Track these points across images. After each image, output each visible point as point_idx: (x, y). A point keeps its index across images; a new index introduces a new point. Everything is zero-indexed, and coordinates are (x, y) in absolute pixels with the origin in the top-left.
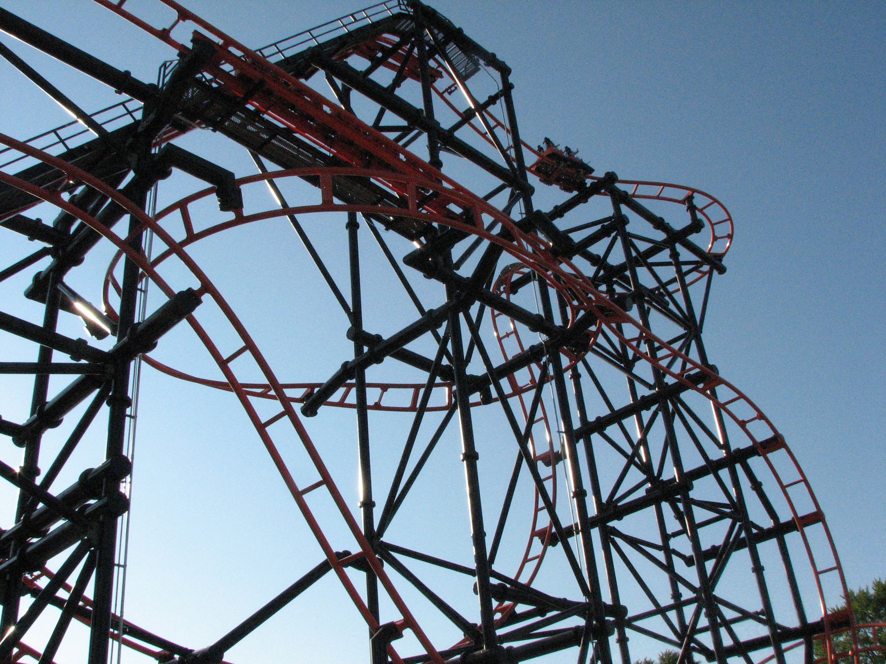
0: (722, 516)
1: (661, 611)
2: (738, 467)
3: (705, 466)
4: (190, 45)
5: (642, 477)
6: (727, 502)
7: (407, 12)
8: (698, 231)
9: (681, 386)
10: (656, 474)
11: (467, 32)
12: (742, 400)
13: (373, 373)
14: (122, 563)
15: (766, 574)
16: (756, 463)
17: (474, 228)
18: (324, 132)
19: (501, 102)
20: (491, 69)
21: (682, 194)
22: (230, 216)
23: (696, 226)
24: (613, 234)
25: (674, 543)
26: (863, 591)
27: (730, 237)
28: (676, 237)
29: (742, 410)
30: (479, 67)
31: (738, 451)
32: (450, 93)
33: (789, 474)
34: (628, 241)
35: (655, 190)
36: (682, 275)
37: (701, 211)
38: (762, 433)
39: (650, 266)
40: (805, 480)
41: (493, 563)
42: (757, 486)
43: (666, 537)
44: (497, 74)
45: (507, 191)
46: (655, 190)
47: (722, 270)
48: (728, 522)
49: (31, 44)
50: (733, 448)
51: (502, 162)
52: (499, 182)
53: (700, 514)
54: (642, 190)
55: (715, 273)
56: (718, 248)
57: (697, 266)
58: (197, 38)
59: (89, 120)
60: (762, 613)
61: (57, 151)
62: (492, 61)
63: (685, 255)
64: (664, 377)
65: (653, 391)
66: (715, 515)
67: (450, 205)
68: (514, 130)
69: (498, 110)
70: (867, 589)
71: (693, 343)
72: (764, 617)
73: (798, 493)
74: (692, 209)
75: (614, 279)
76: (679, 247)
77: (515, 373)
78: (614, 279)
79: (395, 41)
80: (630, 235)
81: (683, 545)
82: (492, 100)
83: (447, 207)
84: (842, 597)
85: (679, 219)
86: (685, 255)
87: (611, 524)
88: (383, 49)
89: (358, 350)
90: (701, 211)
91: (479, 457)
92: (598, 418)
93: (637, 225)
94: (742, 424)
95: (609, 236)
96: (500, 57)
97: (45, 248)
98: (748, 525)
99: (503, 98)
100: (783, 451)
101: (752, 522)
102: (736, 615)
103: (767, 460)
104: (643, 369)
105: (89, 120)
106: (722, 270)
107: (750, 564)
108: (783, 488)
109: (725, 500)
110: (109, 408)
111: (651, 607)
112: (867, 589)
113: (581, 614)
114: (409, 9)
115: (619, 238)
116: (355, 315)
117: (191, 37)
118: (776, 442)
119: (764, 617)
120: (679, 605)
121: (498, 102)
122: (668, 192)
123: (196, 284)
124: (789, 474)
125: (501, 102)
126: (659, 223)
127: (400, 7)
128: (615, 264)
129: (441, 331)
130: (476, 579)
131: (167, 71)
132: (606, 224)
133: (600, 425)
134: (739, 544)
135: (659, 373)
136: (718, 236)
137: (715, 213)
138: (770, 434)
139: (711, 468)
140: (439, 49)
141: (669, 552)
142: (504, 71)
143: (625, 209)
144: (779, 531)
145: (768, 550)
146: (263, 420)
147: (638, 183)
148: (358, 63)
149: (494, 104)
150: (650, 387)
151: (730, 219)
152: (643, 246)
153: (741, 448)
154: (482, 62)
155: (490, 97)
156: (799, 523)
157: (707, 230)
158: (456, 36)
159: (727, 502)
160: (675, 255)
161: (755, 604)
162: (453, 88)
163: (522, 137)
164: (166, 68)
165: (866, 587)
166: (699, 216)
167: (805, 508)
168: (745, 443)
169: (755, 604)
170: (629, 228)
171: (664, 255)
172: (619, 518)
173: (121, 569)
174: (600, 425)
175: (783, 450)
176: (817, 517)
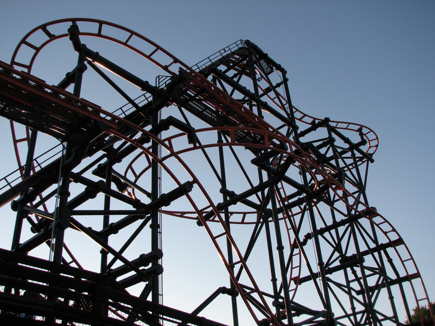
0: (375, 273)
1: (347, 316)
2: (382, 252)
3: (368, 250)
4: (178, 73)
5: (339, 255)
6: (377, 267)
7: (244, 46)
8: (364, 145)
9: (360, 216)
10: (344, 253)
11: (269, 56)
12: (386, 223)
13: (231, 208)
14: (161, 294)
15: (395, 300)
16: (390, 250)
17: (284, 151)
18: (216, 102)
19: (282, 87)
20: (278, 72)
21: (357, 127)
22: (192, 146)
23: (363, 142)
24: (328, 146)
25: (352, 285)
26: (423, 307)
27: (377, 146)
28: (353, 147)
29: (386, 227)
30: (273, 70)
31: (382, 244)
32: (259, 81)
33: (405, 256)
34: (334, 148)
35: (345, 126)
36: (355, 162)
37: (365, 135)
38: (394, 237)
39: (342, 159)
40: (412, 258)
41: (281, 293)
42: (390, 260)
43: (348, 282)
44: (281, 74)
45: (286, 128)
46: (345, 126)
47: (372, 161)
48: (377, 276)
49: (135, 84)
50: (380, 243)
51: (286, 116)
52: (283, 123)
53: (367, 272)
54: (340, 125)
55: (370, 162)
56: (371, 151)
57: (361, 159)
58: (181, 70)
59: (131, 101)
60: (393, 317)
61: (123, 116)
62: (279, 68)
63: (358, 154)
64: (351, 211)
65: (347, 218)
66: (372, 273)
67: (273, 139)
68: (289, 101)
69: (281, 90)
70: (425, 306)
71: (362, 195)
72: (394, 319)
73: (410, 265)
74: (361, 134)
75: (325, 164)
76: (355, 152)
77: (338, 228)
78: (325, 164)
79: (237, 58)
80: (336, 146)
81: (355, 286)
82: (278, 85)
83: (272, 140)
84: (412, 310)
85: (355, 139)
86: (358, 154)
87: (327, 276)
88: (232, 62)
89: (225, 198)
90: (365, 135)
91: (284, 248)
92: (321, 228)
93: (339, 142)
94: (385, 233)
95: (326, 147)
96: (282, 66)
97: (104, 154)
98: (386, 278)
99: (283, 84)
100: (403, 246)
101: (388, 276)
102: (383, 318)
103: (325, 224)
104: (340, 205)
105: (131, 101)
106: (372, 161)
107: (387, 295)
108: (402, 262)
109: (377, 267)
110: (151, 229)
111: (344, 314)
112: (425, 306)
113: (323, 316)
114: (245, 45)
115: (331, 148)
116: (223, 181)
117: (178, 70)
118: (400, 241)
119: (394, 319)
120: (354, 314)
121: (281, 86)
122: (351, 127)
123: (191, 179)
124: (405, 256)
125: (282, 87)
126: (346, 140)
127: (242, 44)
128: (301, 142)
129: (302, 207)
130: (273, 300)
131: (160, 81)
132: (325, 141)
133: (322, 232)
134: (383, 285)
135: (349, 208)
136: (371, 146)
137: (371, 136)
138: (397, 237)
139: (370, 251)
140: (257, 62)
141: (350, 289)
142: (284, 72)
143: (334, 135)
144: (399, 281)
145: (395, 288)
146: (214, 236)
147: (338, 122)
148: (222, 68)
149: (279, 87)
150: (345, 215)
151: (377, 138)
152: (339, 150)
153: (383, 244)
154: (274, 68)
155: (277, 84)
156: (409, 278)
157: (367, 145)
158: (265, 57)
159: (377, 267)
160: (353, 155)
161: (390, 314)
162: (260, 79)
163: (293, 104)
164: (159, 79)
165: (425, 305)
166: (365, 138)
167: (412, 271)
168: (386, 241)
169: (390, 314)
170: (336, 144)
171: (349, 154)
172: (331, 274)
173: (161, 296)
174: (322, 232)
175: (403, 245)
176: (417, 275)
